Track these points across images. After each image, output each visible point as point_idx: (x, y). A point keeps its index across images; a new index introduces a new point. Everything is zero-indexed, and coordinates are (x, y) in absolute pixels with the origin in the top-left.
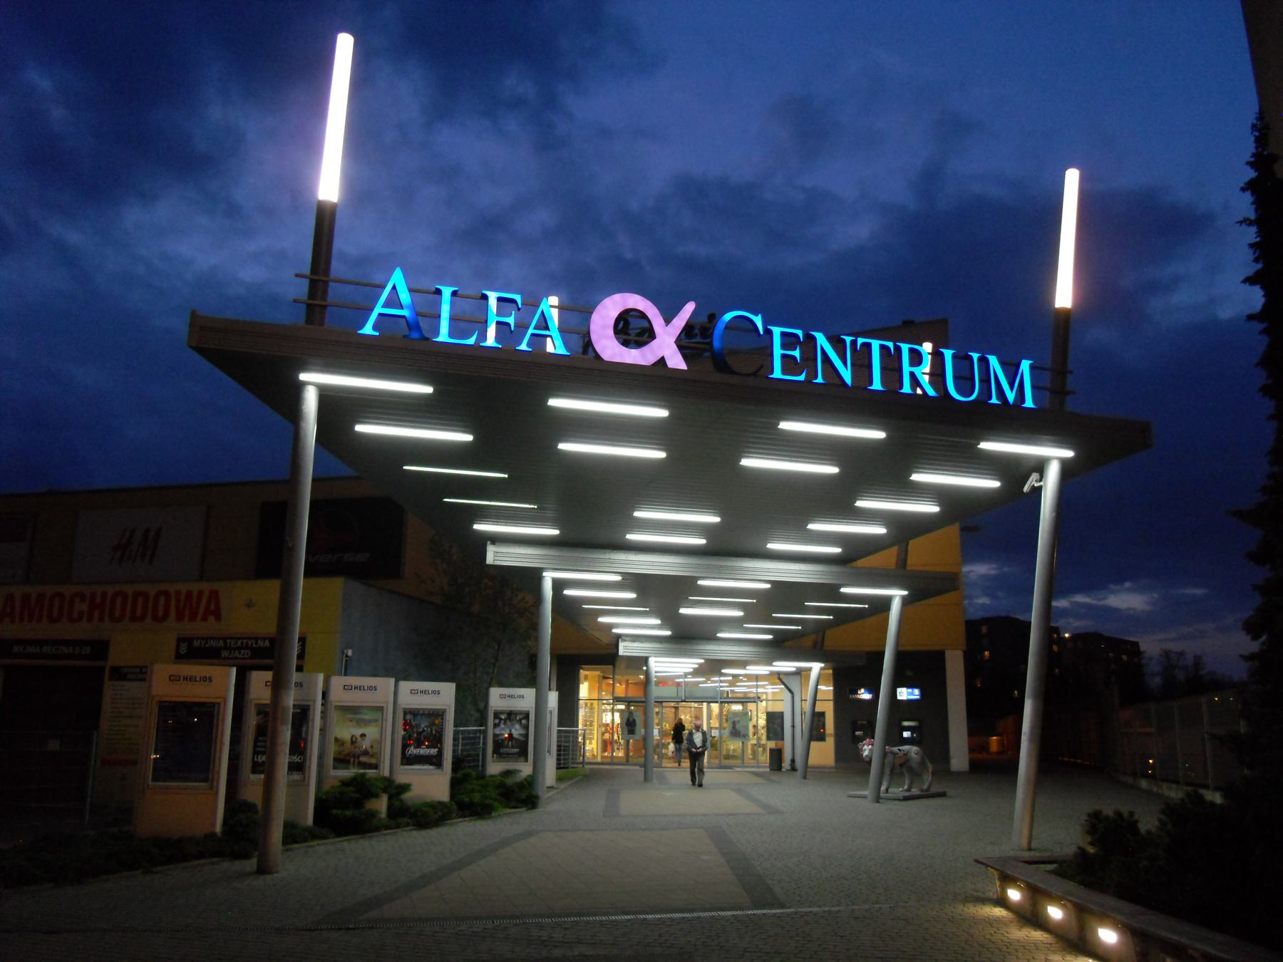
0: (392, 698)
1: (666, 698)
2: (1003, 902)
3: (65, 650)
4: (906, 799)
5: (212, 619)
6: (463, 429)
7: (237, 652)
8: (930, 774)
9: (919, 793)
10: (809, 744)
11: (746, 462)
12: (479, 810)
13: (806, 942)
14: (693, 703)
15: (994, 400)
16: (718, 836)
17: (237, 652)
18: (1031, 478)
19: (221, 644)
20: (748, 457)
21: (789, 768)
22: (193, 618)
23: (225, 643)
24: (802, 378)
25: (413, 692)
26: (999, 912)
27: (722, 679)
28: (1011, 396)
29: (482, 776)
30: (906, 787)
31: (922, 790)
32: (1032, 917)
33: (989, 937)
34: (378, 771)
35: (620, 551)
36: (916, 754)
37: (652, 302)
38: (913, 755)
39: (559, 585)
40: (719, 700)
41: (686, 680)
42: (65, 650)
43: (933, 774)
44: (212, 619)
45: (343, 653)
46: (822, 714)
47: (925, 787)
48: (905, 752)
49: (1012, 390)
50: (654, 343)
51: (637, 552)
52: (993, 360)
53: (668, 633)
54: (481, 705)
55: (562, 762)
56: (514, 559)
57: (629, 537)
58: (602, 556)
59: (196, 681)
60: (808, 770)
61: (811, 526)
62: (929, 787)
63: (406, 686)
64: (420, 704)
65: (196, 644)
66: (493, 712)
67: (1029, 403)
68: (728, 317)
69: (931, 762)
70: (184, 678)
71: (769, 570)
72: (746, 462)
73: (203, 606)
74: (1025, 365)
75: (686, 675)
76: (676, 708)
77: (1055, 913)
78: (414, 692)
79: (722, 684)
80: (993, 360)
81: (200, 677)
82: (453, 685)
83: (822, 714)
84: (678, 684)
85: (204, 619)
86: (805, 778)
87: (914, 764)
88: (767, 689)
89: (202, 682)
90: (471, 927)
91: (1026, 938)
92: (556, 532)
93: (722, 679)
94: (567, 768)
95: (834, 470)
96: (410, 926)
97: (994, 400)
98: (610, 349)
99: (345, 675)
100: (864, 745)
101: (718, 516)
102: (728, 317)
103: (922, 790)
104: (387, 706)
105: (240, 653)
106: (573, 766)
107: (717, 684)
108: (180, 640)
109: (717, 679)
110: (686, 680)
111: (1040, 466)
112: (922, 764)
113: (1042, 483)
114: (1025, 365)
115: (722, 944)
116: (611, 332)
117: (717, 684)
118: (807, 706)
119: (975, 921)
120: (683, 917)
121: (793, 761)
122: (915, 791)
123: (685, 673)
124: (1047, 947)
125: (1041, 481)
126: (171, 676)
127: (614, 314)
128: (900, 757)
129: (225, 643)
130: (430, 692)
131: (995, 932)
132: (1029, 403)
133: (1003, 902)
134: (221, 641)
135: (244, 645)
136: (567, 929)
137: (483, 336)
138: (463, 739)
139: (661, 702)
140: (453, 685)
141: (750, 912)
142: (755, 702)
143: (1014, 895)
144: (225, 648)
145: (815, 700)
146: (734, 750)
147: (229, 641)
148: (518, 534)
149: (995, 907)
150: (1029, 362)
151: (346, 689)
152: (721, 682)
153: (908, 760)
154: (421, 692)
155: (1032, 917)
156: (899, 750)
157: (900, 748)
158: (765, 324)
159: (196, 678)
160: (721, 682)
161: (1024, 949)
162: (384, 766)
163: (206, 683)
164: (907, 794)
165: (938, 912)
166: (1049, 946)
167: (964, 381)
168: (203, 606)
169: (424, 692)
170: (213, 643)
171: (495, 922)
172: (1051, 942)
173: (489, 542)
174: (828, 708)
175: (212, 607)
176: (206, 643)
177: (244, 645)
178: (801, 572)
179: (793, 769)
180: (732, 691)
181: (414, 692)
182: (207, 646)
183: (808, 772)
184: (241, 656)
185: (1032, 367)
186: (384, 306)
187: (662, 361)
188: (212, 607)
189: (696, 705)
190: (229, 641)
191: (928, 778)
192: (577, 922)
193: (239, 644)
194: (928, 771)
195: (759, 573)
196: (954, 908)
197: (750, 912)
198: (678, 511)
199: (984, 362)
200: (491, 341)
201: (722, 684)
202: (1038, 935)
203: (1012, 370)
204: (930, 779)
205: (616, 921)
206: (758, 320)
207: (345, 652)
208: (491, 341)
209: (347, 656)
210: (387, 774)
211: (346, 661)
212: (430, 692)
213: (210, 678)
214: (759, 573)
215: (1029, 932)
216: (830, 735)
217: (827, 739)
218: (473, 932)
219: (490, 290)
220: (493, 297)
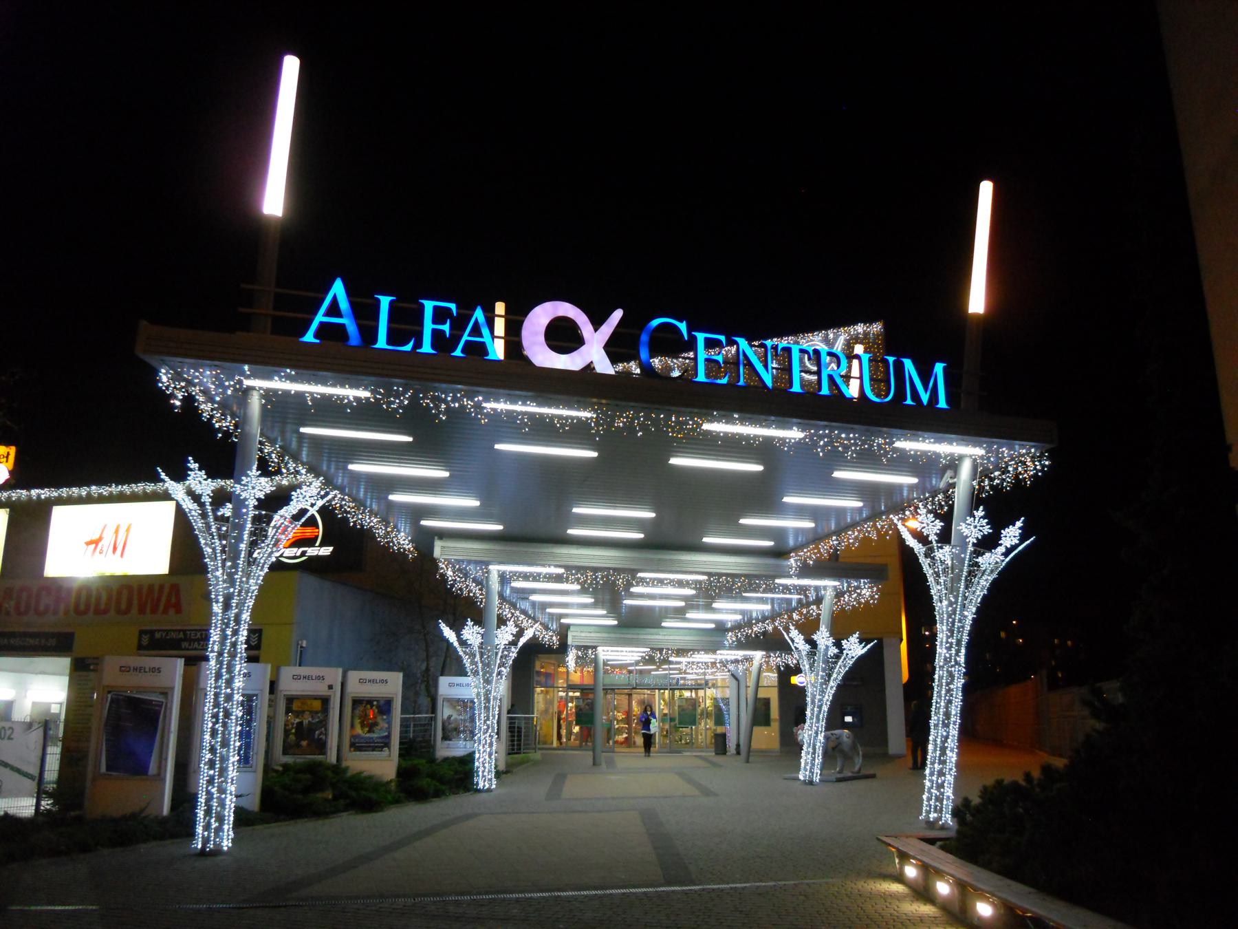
0: (340, 687)
1: (620, 685)
2: (900, 878)
3: (31, 641)
4: (839, 780)
5: (172, 611)
6: (588, 447)
7: (196, 643)
8: (861, 758)
9: (850, 774)
10: (752, 731)
11: (674, 461)
12: (420, 796)
13: (706, 917)
14: (646, 690)
15: (909, 402)
16: (649, 818)
17: (196, 643)
18: (946, 475)
19: (181, 635)
20: (677, 456)
21: (734, 752)
22: (154, 610)
23: (185, 635)
24: (724, 381)
25: (295, 677)
26: (897, 888)
27: (671, 666)
28: (925, 397)
29: (432, 760)
30: (838, 769)
31: (853, 772)
32: (923, 893)
33: (880, 911)
34: (325, 756)
35: (571, 546)
36: (848, 738)
37: (537, 306)
38: (845, 739)
39: (504, 579)
40: (669, 688)
41: (637, 668)
42: (31, 641)
43: (864, 756)
44: (172, 611)
45: (298, 644)
46: (767, 702)
47: (856, 769)
48: (837, 736)
49: (926, 391)
50: (583, 348)
51: (579, 546)
52: (908, 364)
53: (615, 622)
54: (432, 690)
55: (516, 747)
56: (589, 561)
57: (705, 540)
58: (546, 550)
59: (145, 672)
60: (751, 754)
61: (742, 521)
62: (860, 769)
63: (354, 676)
64: (303, 691)
65: (158, 635)
66: (350, 699)
67: (942, 404)
68: (656, 322)
69: (861, 746)
70: (134, 669)
71: (712, 563)
72: (674, 461)
73: (164, 599)
74: (939, 368)
75: (637, 663)
76: (630, 695)
77: (943, 888)
78: (362, 681)
79: (671, 672)
80: (908, 364)
81: (150, 668)
82: (401, 675)
83: (767, 702)
84: (630, 672)
85: (165, 611)
86: (747, 761)
87: (846, 748)
88: (717, 676)
89: (151, 673)
90: (392, 904)
91: (915, 912)
92: (500, 527)
93: (671, 666)
94: (520, 753)
95: (595, 454)
96: (334, 904)
97: (909, 402)
98: (544, 357)
99: (300, 665)
100: (799, 730)
101: (652, 512)
102: (656, 322)
103: (853, 772)
104: (396, 697)
105: (199, 644)
106: (525, 751)
107: (667, 672)
108: (142, 632)
109: (666, 667)
110: (637, 668)
111: (954, 464)
112: (854, 747)
113: (955, 480)
114: (939, 368)
115: (698, 923)
116: (542, 338)
117: (667, 672)
118: (751, 691)
119: (871, 896)
120: (596, 894)
121: (738, 745)
122: (847, 773)
123: (636, 661)
124: (932, 921)
125: (955, 477)
126: (360, 679)
127: (545, 321)
128: (833, 741)
129: (185, 635)
130: (378, 681)
131: (887, 907)
132: (942, 404)
133: (900, 878)
134: (182, 633)
135: (203, 636)
136: (482, 905)
137: (419, 344)
138: (415, 726)
139: (613, 689)
140: (401, 675)
141: (662, 889)
142: (703, 689)
143: (911, 872)
144: (185, 639)
145: (757, 686)
146: (360, 719)
147: (188, 632)
148: (612, 538)
149: (893, 883)
150: (943, 365)
151: (123, 671)
152: (671, 669)
153: (840, 744)
154: (370, 681)
155: (923, 893)
156: (832, 734)
157: (833, 732)
158: (689, 330)
159: (145, 668)
160: (671, 669)
161: (903, 925)
162: (331, 753)
163: (156, 673)
164: (839, 776)
165: (839, 888)
166: (933, 919)
167: (879, 381)
168: (164, 599)
169: (373, 681)
170: (173, 635)
171: (416, 899)
172: (937, 916)
173: (436, 538)
174: (773, 696)
175: (173, 600)
176: (167, 635)
177: (203, 636)
178: (737, 564)
179: (738, 753)
180: (684, 679)
181: (362, 681)
182: (168, 637)
183: (746, 753)
184: (200, 647)
185: (945, 370)
186: (326, 315)
187: (589, 368)
188: (173, 600)
189: (649, 692)
190: (188, 632)
191: (858, 761)
192: (494, 900)
193: (199, 636)
194: (859, 754)
195: (701, 566)
196: (855, 884)
197: (662, 889)
198: (615, 508)
199: (899, 367)
200: (427, 348)
201: (671, 672)
202: (926, 909)
203: (925, 375)
204: (861, 761)
205: (531, 898)
206: (683, 327)
207: (300, 642)
208: (427, 348)
209: (302, 647)
210: (332, 757)
211: (301, 651)
212: (378, 681)
213: (158, 668)
214: (701, 566)
215: (919, 907)
216: (775, 720)
217: (772, 724)
218: (394, 909)
219: (426, 299)
220: (429, 306)
